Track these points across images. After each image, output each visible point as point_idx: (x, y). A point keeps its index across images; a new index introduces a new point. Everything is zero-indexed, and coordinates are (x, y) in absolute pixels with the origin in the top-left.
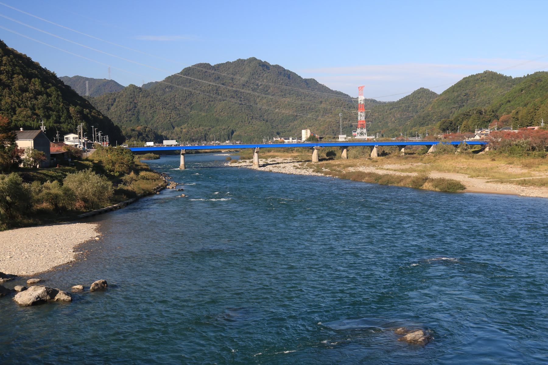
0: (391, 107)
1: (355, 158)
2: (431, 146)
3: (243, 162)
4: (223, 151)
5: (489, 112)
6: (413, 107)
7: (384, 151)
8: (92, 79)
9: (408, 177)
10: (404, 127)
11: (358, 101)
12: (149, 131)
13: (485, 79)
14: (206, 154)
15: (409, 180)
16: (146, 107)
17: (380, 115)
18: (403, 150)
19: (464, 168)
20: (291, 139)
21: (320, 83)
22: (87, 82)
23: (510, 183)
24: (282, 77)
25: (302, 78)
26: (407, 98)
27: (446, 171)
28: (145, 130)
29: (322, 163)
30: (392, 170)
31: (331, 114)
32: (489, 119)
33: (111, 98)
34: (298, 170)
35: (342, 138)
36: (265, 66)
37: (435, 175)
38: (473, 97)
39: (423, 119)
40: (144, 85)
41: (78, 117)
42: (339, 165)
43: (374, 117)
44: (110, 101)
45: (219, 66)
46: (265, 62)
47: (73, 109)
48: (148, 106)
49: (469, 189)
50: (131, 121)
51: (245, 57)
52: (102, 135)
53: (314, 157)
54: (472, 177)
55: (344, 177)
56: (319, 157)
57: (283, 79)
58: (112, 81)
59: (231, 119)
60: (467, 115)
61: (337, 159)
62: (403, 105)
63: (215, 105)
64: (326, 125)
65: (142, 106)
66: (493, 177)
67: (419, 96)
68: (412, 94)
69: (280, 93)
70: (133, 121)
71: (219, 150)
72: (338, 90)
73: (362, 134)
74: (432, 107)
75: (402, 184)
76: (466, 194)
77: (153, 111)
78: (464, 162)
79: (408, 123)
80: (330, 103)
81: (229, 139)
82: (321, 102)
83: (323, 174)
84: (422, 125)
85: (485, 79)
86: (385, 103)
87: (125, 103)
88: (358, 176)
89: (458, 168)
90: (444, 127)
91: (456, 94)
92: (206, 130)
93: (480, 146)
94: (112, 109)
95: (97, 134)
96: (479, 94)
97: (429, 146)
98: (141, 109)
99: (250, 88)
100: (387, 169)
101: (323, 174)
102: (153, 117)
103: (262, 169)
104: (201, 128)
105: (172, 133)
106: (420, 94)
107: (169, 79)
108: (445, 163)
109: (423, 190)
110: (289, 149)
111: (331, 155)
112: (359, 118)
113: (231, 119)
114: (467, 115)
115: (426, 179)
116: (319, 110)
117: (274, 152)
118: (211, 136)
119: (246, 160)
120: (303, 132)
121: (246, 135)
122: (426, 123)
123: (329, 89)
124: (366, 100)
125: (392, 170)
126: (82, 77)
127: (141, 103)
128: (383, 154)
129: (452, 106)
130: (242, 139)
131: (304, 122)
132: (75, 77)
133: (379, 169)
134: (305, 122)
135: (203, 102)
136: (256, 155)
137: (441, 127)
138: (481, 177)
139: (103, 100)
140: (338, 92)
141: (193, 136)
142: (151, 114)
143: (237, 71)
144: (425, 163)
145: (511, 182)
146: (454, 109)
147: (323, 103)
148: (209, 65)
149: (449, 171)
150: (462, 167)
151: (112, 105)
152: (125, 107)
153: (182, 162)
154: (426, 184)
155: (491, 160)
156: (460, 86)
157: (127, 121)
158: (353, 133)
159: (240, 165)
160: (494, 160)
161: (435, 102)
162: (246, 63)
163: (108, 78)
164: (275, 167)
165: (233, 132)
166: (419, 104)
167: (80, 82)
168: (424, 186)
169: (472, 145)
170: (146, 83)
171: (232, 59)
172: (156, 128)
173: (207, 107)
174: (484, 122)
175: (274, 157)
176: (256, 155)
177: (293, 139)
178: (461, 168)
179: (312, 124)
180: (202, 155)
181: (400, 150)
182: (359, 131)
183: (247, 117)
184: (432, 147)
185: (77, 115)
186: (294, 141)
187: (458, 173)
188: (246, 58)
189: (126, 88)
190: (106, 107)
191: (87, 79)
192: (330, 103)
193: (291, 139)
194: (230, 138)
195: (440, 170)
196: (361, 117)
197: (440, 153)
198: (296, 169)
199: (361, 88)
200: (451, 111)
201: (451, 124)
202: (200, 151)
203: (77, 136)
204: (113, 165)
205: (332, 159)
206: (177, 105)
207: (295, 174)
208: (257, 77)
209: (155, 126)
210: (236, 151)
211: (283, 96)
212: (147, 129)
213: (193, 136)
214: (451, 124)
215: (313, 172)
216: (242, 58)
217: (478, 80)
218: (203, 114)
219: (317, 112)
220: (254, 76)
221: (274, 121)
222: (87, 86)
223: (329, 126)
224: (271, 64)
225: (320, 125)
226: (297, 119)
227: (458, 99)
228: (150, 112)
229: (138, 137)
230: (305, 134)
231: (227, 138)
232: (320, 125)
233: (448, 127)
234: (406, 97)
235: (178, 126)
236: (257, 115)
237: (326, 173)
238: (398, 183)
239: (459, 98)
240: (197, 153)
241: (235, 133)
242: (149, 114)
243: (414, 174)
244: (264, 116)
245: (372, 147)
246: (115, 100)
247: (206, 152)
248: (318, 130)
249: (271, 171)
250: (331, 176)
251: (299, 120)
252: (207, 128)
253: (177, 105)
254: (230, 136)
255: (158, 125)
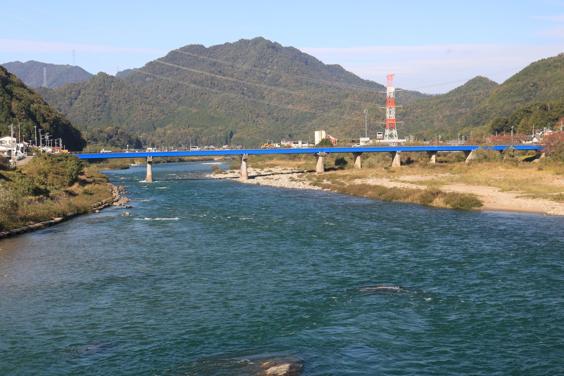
0: (438, 101)
1: (370, 167)
2: (470, 151)
3: (231, 172)
4: (215, 159)
5: (557, 107)
6: (467, 101)
7: (409, 159)
8: (51, 65)
9: (419, 191)
10: (453, 127)
11: (386, 94)
12: (122, 133)
13: (560, 64)
14: (192, 163)
15: (417, 196)
16: (120, 101)
17: (424, 112)
18: (433, 157)
19: (500, 179)
20: (300, 143)
21: (347, 69)
22: (45, 69)
23: (544, 198)
24: (298, 62)
25: (323, 64)
26: (458, 90)
27: (476, 184)
28: (117, 131)
29: (327, 173)
30: (409, 182)
31: (360, 111)
32: (556, 117)
33: (74, 90)
34: (294, 183)
35: (364, 141)
36: (275, 47)
37: (448, 189)
38: (544, 89)
39: (478, 117)
40: (119, 73)
41: (22, 115)
42: (344, 177)
43: (415, 114)
44: (73, 93)
45: (215, 48)
46: (275, 43)
47: (17, 104)
48: (122, 100)
49: (486, 205)
50: (99, 119)
51: (250, 37)
52: (50, 138)
53: (319, 167)
54: (503, 191)
55: (343, 191)
56: (325, 165)
57: (298, 65)
58: (77, 67)
59: (230, 117)
60: (528, 112)
61: (348, 169)
62: (454, 98)
63: (210, 99)
64: (354, 126)
65: (114, 101)
66: (529, 191)
67: (475, 88)
68: (465, 84)
69: (294, 84)
70: (102, 120)
71: (211, 157)
72: (370, 80)
73: (391, 136)
74: (490, 101)
75: (409, 200)
76: (485, 211)
77: (129, 106)
78: (502, 171)
79: (459, 122)
80: (359, 96)
81: (227, 143)
82: (347, 95)
83: (320, 188)
84: (477, 124)
85: (560, 64)
86: (431, 96)
87: (93, 96)
88: (360, 189)
89: (493, 179)
90: (497, 127)
91: (521, 83)
92: (196, 132)
93: (534, 151)
94: (76, 104)
95: (43, 137)
96: (551, 84)
97: (467, 152)
98: (113, 105)
99: (256, 77)
100: (403, 182)
101: (320, 188)
102: (129, 114)
103: (250, 181)
104: (191, 128)
105: (153, 135)
106: (476, 85)
107: (151, 65)
108: (479, 173)
109: (432, 207)
110: (293, 155)
111: (341, 163)
112: (388, 115)
113: (230, 117)
114: (528, 112)
115: (438, 193)
116: (345, 105)
117: (277, 159)
118: (204, 139)
119: (234, 170)
120: (317, 133)
121: (249, 138)
122: (482, 122)
123: (359, 78)
124: (398, 92)
125: (409, 182)
126: (38, 62)
127: (113, 97)
128: (409, 162)
129: (516, 99)
130: (244, 144)
131: (325, 121)
132: (29, 62)
133: (394, 181)
134: (326, 121)
135: (194, 95)
136: (244, 163)
137: (494, 127)
138: (514, 191)
139: (63, 93)
140: (370, 82)
141: (180, 140)
142: (126, 110)
143: (239, 54)
144: (454, 174)
145: (545, 197)
146: (519, 104)
147: (350, 96)
148: (202, 46)
149: (479, 183)
150: (498, 178)
151: (76, 99)
152: (92, 102)
153: (149, 173)
154: (437, 199)
155: (537, 168)
156: (526, 74)
157: (95, 120)
158: (378, 135)
159: (226, 176)
160: (541, 169)
161: (494, 95)
162: (250, 43)
163: (72, 63)
164: (268, 178)
165: (232, 134)
166: (475, 97)
167: (35, 69)
168: (434, 202)
169: (525, 150)
170: (122, 70)
171: (233, 39)
172: (133, 129)
173: (199, 101)
174: (550, 120)
175: (272, 166)
176: (244, 163)
177: (303, 143)
178: (496, 180)
179: (334, 124)
180: (187, 164)
181: (430, 157)
182: (387, 132)
183: (250, 114)
184: (471, 153)
185: (22, 112)
186: (304, 145)
187: (489, 185)
188: (250, 39)
189: (94, 77)
190: (68, 102)
191: (45, 65)
192: (359, 96)
193: (300, 143)
194: (228, 141)
195: (467, 182)
196: (391, 114)
197: (480, 161)
198: (291, 181)
199: (390, 77)
200: (514, 106)
201: (507, 123)
202: (186, 158)
203: (15, 139)
204: (46, 176)
205: (342, 168)
206: (161, 99)
207: (286, 188)
208: (264, 62)
209: (131, 126)
210: (233, 159)
211: (298, 87)
212: (120, 130)
213: (180, 140)
214: (507, 123)
215: (310, 185)
216: (245, 38)
217: (549, 66)
218: (195, 111)
219: (342, 108)
220: (261, 61)
221: (286, 120)
222: (45, 74)
223: (357, 127)
224: (284, 45)
225: (345, 126)
226: (316, 118)
227: (523, 91)
228: (125, 108)
229: (108, 140)
230: (319, 136)
231: (225, 142)
232: (345, 126)
233: (502, 128)
234: (458, 88)
235: (161, 126)
236: (264, 112)
237: (328, 186)
238: (405, 198)
239: (526, 90)
240: (181, 160)
241: (235, 136)
242: (123, 110)
243: (423, 188)
244: (273, 114)
245: (393, 154)
246: (80, 93)
247: (193, 161)
248: (342, 131)
249: (258, 184)
250: (329, 189)
251: (319, 118)
252: (198, 129)
253: (161, 99)
254: (229, 139)
255: (135, 124)
